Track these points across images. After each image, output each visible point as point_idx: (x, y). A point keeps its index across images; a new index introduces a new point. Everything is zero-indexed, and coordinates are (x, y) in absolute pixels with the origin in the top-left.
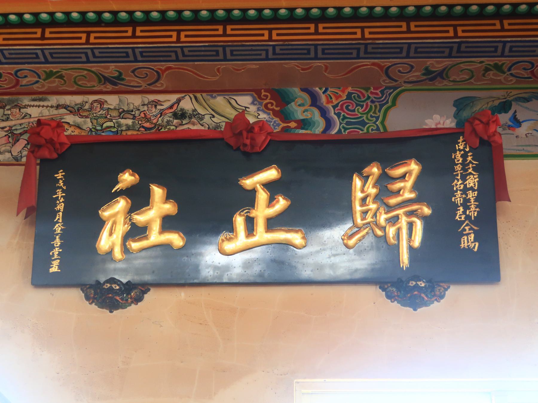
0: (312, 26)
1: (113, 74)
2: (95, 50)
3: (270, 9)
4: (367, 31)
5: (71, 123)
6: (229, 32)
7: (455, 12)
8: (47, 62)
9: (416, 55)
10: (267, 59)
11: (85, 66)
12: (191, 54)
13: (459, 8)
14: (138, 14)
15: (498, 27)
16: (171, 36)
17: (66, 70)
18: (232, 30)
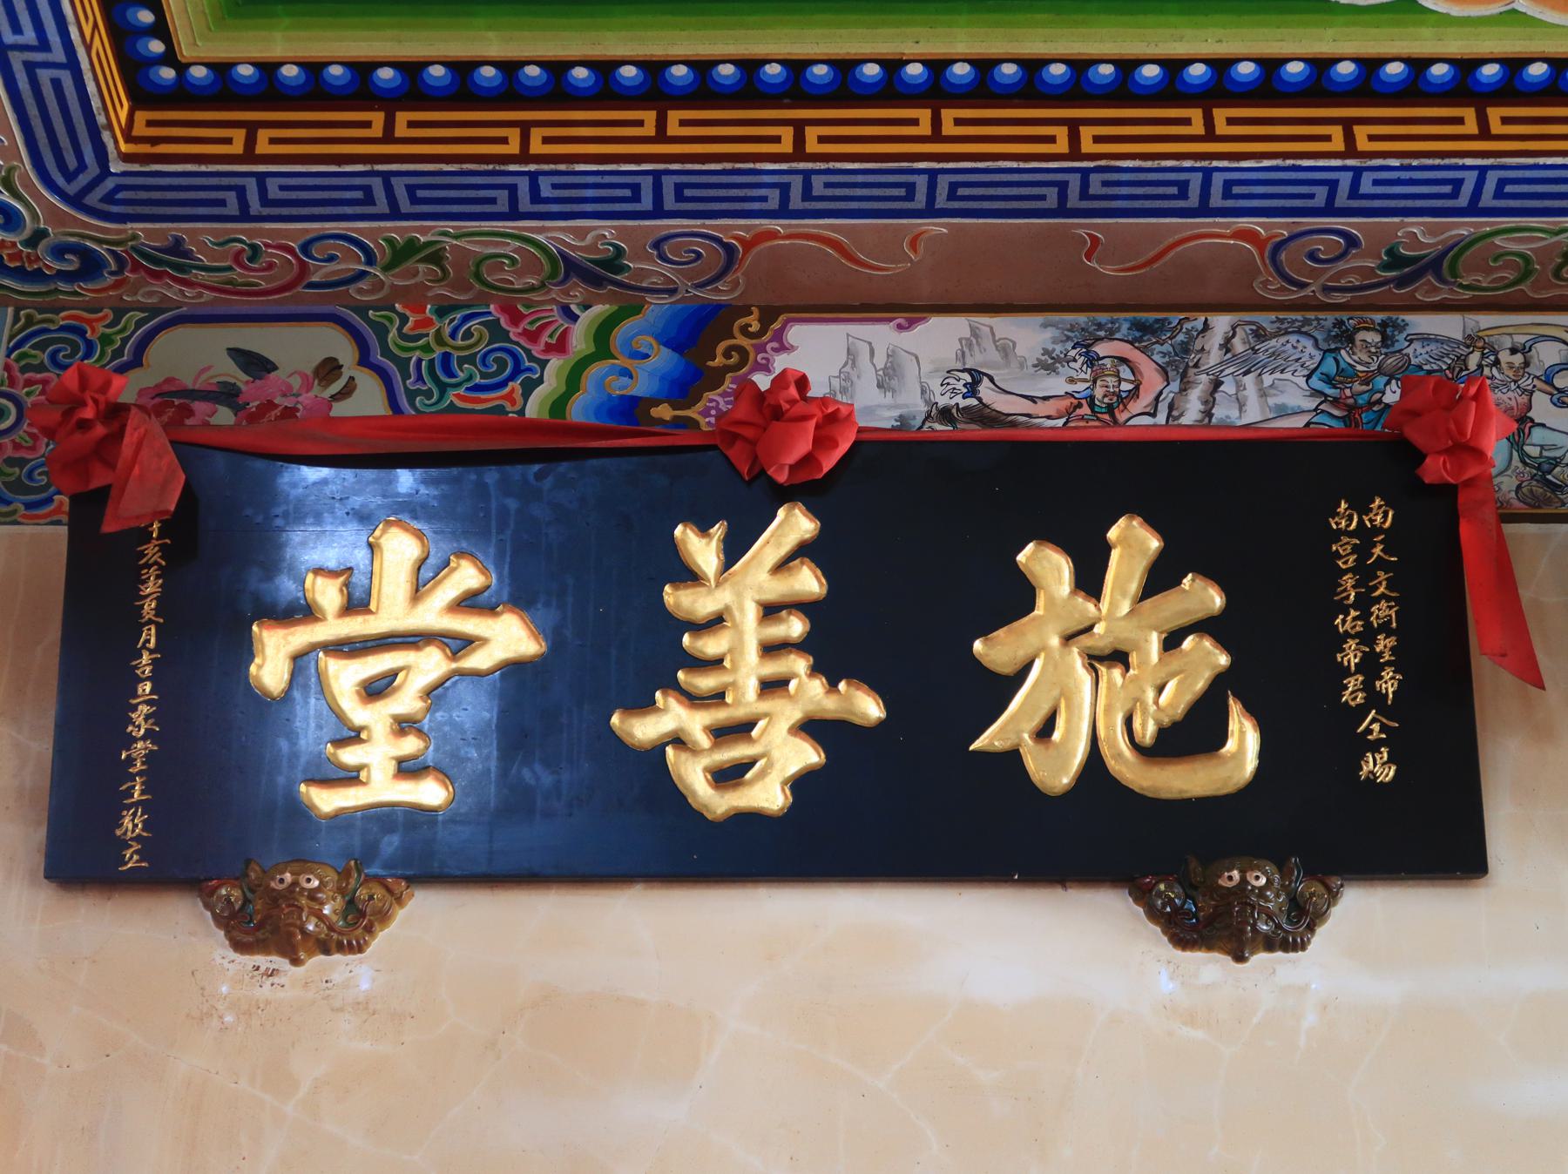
0: (377, 118)
1: (598, 251)
2: (394, 180)
3: (252, 64)
4: (1086, 133)
5: (1053, 413)
6: (673, 129)
7: (1484, 81)
8: (395, 214)
9: (1230, 203)
10: (1062, 211)
11: (815, 226)
12: (830, 192)
13: (580, 73)
14: (290, 71)
15: (1471, 127)
16: (822, 140)
17: (456, 237)
18: (683, 123)
